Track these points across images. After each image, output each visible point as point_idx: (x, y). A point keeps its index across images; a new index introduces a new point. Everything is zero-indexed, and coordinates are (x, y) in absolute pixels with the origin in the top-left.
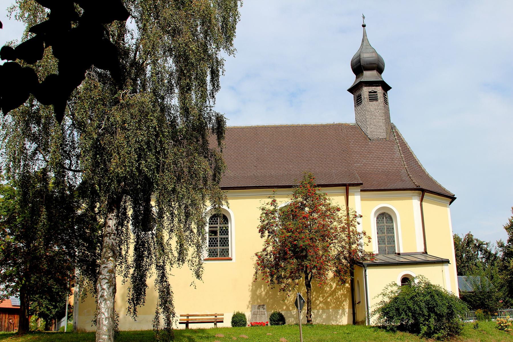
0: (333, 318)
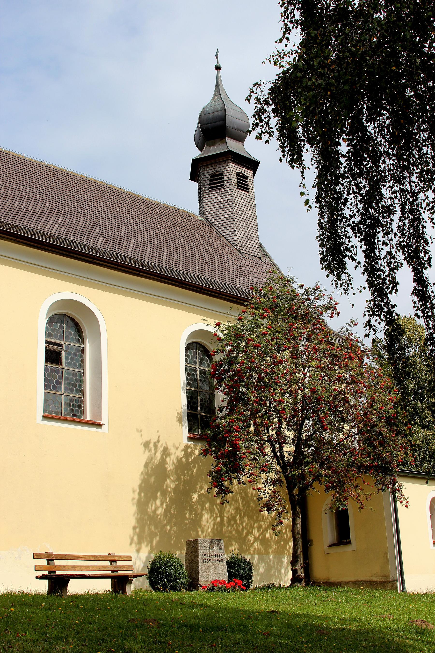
0: (274, 572)
